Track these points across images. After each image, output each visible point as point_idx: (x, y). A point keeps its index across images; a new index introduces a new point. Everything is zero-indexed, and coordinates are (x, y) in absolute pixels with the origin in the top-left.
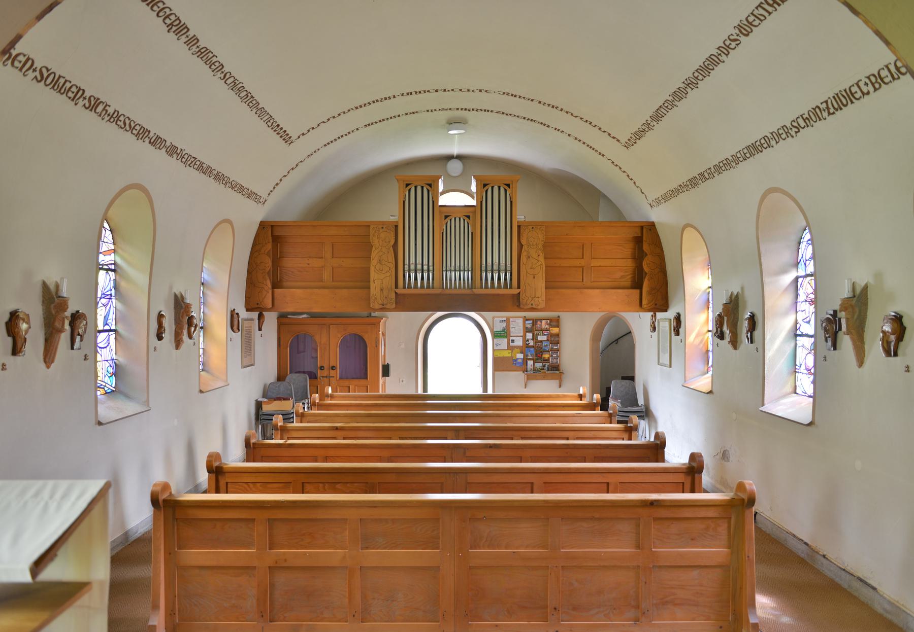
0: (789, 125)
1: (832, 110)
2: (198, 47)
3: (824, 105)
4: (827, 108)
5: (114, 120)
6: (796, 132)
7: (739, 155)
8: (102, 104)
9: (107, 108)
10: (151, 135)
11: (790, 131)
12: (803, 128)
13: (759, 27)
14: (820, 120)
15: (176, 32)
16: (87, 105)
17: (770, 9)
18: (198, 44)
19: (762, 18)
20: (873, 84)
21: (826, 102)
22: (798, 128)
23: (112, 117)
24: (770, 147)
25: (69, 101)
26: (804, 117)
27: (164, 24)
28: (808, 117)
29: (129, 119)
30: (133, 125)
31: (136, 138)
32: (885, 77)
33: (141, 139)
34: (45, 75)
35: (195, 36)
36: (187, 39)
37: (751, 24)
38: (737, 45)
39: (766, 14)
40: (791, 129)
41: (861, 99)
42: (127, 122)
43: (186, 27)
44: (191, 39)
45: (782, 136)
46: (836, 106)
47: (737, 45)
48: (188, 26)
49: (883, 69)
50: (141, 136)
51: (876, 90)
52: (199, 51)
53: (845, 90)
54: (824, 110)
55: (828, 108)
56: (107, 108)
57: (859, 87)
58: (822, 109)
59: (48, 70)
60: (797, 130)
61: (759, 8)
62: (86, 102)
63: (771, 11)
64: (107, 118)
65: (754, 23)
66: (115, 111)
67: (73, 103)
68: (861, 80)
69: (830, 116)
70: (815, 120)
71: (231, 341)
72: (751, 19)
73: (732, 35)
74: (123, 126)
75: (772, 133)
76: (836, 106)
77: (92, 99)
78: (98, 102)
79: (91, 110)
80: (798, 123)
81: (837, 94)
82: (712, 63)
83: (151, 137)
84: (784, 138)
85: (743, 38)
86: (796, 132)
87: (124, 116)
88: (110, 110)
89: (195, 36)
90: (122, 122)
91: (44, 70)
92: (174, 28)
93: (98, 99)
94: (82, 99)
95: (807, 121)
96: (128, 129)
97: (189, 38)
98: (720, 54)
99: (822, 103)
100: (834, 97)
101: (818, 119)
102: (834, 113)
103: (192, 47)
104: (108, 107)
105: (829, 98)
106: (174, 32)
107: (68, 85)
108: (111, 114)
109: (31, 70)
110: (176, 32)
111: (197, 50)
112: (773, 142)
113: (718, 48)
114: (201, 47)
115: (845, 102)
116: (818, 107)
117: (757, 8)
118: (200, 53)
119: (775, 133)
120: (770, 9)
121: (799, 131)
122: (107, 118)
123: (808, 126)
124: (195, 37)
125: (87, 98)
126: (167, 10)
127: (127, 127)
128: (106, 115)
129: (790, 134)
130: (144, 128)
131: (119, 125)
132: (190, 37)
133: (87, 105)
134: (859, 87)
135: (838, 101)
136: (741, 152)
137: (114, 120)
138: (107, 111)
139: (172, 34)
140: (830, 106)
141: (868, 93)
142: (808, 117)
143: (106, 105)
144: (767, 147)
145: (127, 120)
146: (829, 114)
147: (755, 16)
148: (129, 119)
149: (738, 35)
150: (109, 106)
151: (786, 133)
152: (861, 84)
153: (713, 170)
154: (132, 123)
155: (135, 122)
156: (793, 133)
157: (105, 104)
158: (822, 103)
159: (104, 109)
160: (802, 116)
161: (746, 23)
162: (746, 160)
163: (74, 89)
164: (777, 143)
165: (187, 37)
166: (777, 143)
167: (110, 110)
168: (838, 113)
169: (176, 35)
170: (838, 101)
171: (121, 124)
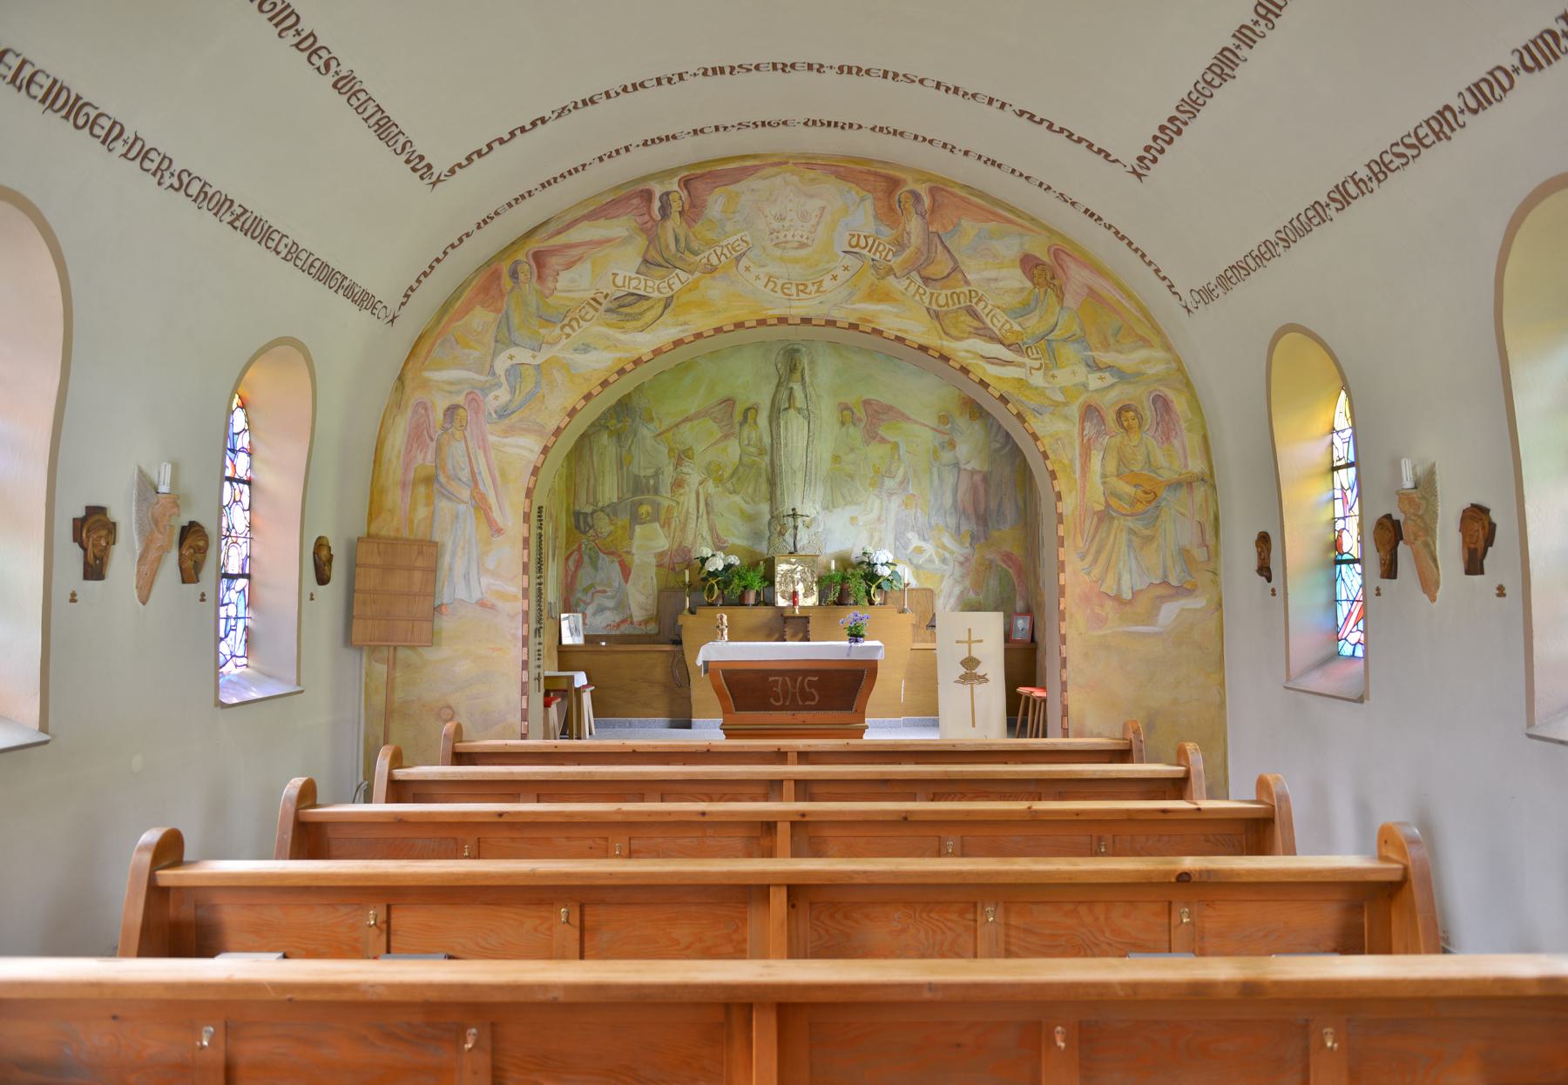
0: (177, 168)
1: (238, 224)
2: (1256, 23)
3: (239, 211)
4: (238, 220)
5: (1384, 172)
6: (171, 186)
7: (303, 256)
8: (1346, 184)
9: (1357, 178)
10: (1456, 104)
11: (167, 174)
12: (187, 195)
13: (347, 104)
14: (216, 214)
15: (1251, 44)
16: (1339, 206)
17: (372, 121)
18: (1250, 24)
19: (360, 110)
20: (289, 252)
21: (245, 211)
22: (181, 187)
23: (1376, 175)
24: (103, 142)
25: (1323, 225)
26: (207, 189)
27: (1222, 86)
28: (209, 195)
29: (1397, 144)
30: (1413, 140)
31: (1445, 140)
32: (37, 83)
33: (1453, 130)
34: (1283, 236)
35: (1234, 36)
36: (1243, 46)
37: (355, 94)
38: (318, 69)
39: (366, 115)
40: (172, 175)
41: (269, 250)
42: (1401, 149)
43: (1221, 53)
44: (1240, 40)
45: (312, 268)
46: (246, 226)
47: (318, 69)
48: (1237, 28)
49: (159, 154)
50: (1446, 129)
51: (285, 258)
52: (1264, 17)
53: (270, 227)
54: (232, 214)
55: (238, 218)
56: (1357, 178)
57: (280, 240)
58: (232, 209)
59: (1280, 231)
60: (177, 185)
61: (376, 109)
62: (1333, 205)
63: (369, 121)
64: (1374, 184)
65: (354, 98)
66: (1369, 166)
67: (1368, 194)
68: (288, 237)
69: (230, 226)
70: (211, 206)
71: (1378, 594)
72: (362, 96)
73: (339, 65)
74: (1404, 160)
75: (137, 138)
76: (246, 226)
77: (1332, 195)
78: (1341, 189)
79: (1349, 203)
80: (190, 182)
81: (261, 220)
82: (386, 130)
83: (1463, 107)
84: (269, 245)
85: (330, 79)
86: (171, 186)
87: (1386, 152)
88: (1363, 173)
89: (1234, 36)
90: (1394, 159)
91: (1279, 235)
92: (1227, 70)
93: (1337, 187)
94: (1327, 210)
95: (202, 196)
96: (1415, 152)
97: (1241, 44)
98: (298, 33)
99: (240, 206)
100: (256, 218)
101: (215, 211)
102: (235, 228)
103: (1240, 56)
104: (1355, 177)
105: (252, 212)
106: (1233, 69)
107: (1303, 218)
108: (1371, 175)
109: (1276, 247)
110: (1251, 44)
111: (1262, 22)
112: (120, 147)
113: (312, 34)
114: (1256, 18)
115: (256, 234)
116: (232, 202)
117: (378, 106)
118: (1270, 16)
119: (143, 146)
120: (372, 121)
121: (177, 190)
122: (1374, 184)
123: (195, 201)
124: (1237, 34)
125: (1328, 201)
126: (1199, 87)
127: (1410, 152)
128: (1369, 184)
129: (162, 177)
130: (1433, 118)
131: (1398, 168)
132: (1237, 42)
133: (1339, 206)
134: (280, 240)
135: (254, 225)
136: (311, 259)
137: (1384, 172)
138: (1361, 180)
139: (1237, 72)
140: (242, 219)
141: (278, 253)
142: (209, 195)
143: (1352, 177)
144: (311, 274)
145: (1395, 149)
146: (231, 223)
147: (365, 102)
148: (1397, 144)
149: (336, 73)
150: (1356, 173)
151: (158, 168)
152: (285, 240)
153: (346, 283)
154: (1407, 141)
155: (1409, 135)
156: (167, 181)
157: (1349, 179)
158: (240, 206)
159: (1356, 184)
160: (205, 183)
161: (356, 88)
162: (303, 271)
163: (1311, 213)
164: (125, 155)
165: (1238, 47)
166: (125, 155)
167: (1363, 173)
168: (240, 234)
169: (1237, 65)
170: (254, 225)
171: (1398, 162)
